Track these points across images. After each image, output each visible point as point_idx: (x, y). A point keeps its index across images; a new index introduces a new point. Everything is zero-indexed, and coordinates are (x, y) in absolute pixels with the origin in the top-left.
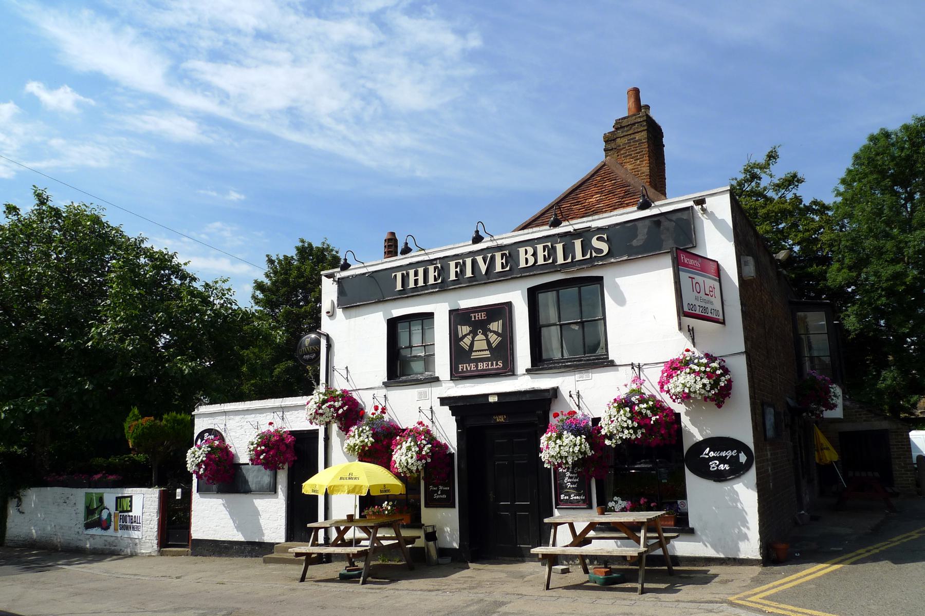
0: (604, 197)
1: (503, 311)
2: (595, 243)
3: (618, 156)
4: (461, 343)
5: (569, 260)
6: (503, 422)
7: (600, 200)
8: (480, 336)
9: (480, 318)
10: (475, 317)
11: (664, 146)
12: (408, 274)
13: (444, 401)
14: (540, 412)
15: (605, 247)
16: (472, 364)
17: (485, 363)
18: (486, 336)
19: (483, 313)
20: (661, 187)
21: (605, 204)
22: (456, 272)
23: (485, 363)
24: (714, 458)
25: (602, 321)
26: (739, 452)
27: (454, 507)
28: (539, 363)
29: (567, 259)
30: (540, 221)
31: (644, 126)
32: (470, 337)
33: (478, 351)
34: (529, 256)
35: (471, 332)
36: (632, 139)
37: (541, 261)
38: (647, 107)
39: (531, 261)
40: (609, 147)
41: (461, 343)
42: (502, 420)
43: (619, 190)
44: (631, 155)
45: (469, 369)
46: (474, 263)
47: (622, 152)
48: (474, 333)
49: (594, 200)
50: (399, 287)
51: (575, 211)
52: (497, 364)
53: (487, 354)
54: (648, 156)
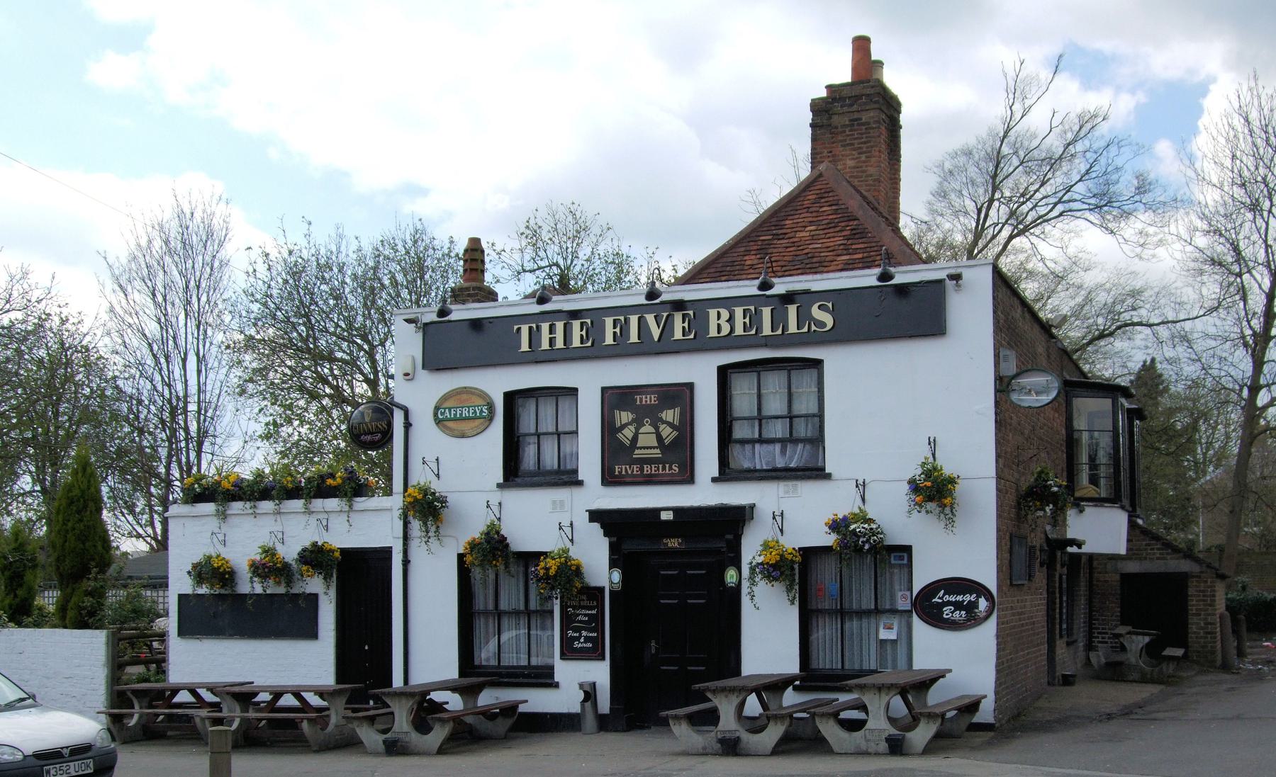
0: (821, 232)
1: (681, 395)
2: (816, 312)
4: (620, 435)
5: (779, 332)
6: (676, 548)
8: (647, 428)
9: (648, 402)
10: (641, 399)
11: (901, 127)
12: (538, 328)
13: (595, 516)
14: (729, 537)
15: (828, 320)
16: (635, 466)
17: (653, 466)
18: (657, 428)
19: (653, 396)
22: (615, 333)
23: (653, 466)
24: (949, 603)
25: (817, 419)
26: (979, 597)
27: (603, 659)
28: (727, 473)
29: (778, 329)
30: (729, 260)
32: (632, 428)
33: (644, 448)
34: (723, 322)
35: (634, 421)
36: (856, 120)
37: (739, 330)
39: (726, 329)
41: (620, 435)
42: (676, 545)
44: (853, 144)
45: (630, 472)
47: (840, 138)
48: (638, 423)
50: (525, 347)
51: (780, 250)
52: (671, 468)
53: (656, 453)
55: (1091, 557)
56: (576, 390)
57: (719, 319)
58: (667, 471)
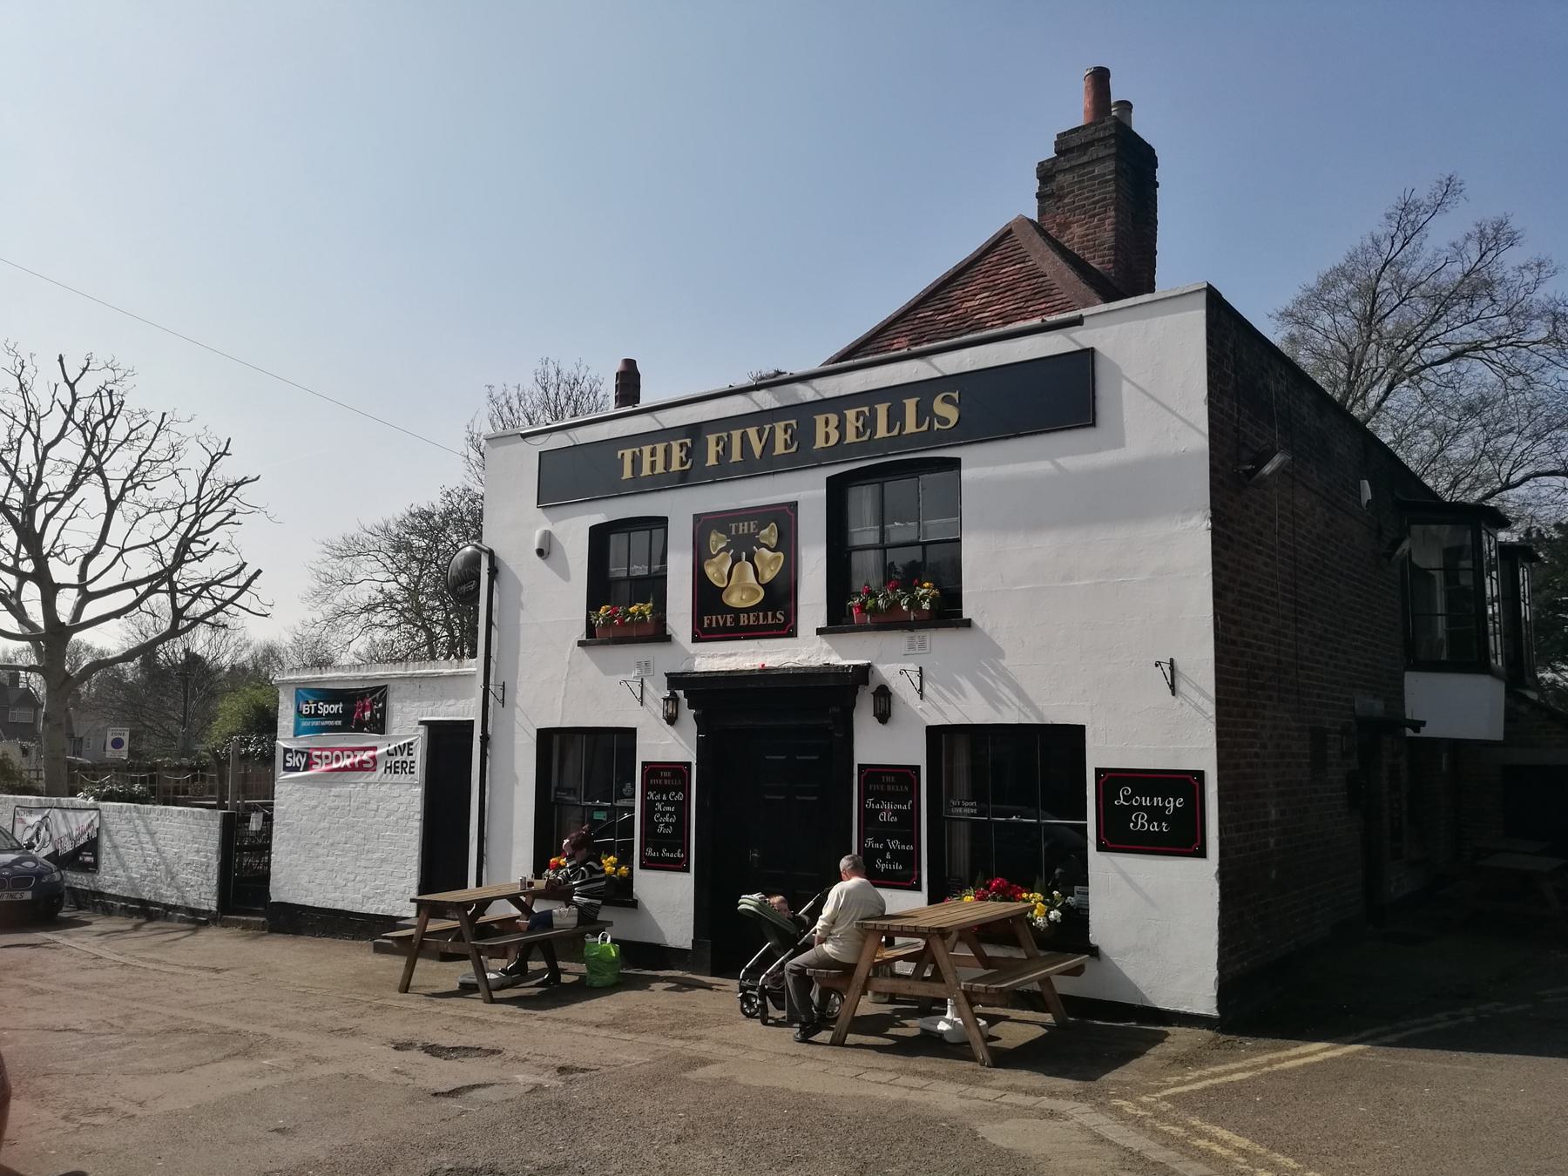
3: (1058, 208)
5: (895, 432)
7: (986, 305)
10: (737, 528)
14: (835, 710)
20: (245, 789)
21: (994, 313)
24: (1140, 808)
28: (838, 620)
31: (1111, 146)
37: (851, 437)
38: (1126, 106)
40: (1047, 189)
43: (1024, 284)
46: (745, 439)
49: (977, 302)
50: (627, 474)
54: (1115, 210)
55: (1434, 742)
56: (666, 519)
57: (827, 426)
58: (770, 621)
